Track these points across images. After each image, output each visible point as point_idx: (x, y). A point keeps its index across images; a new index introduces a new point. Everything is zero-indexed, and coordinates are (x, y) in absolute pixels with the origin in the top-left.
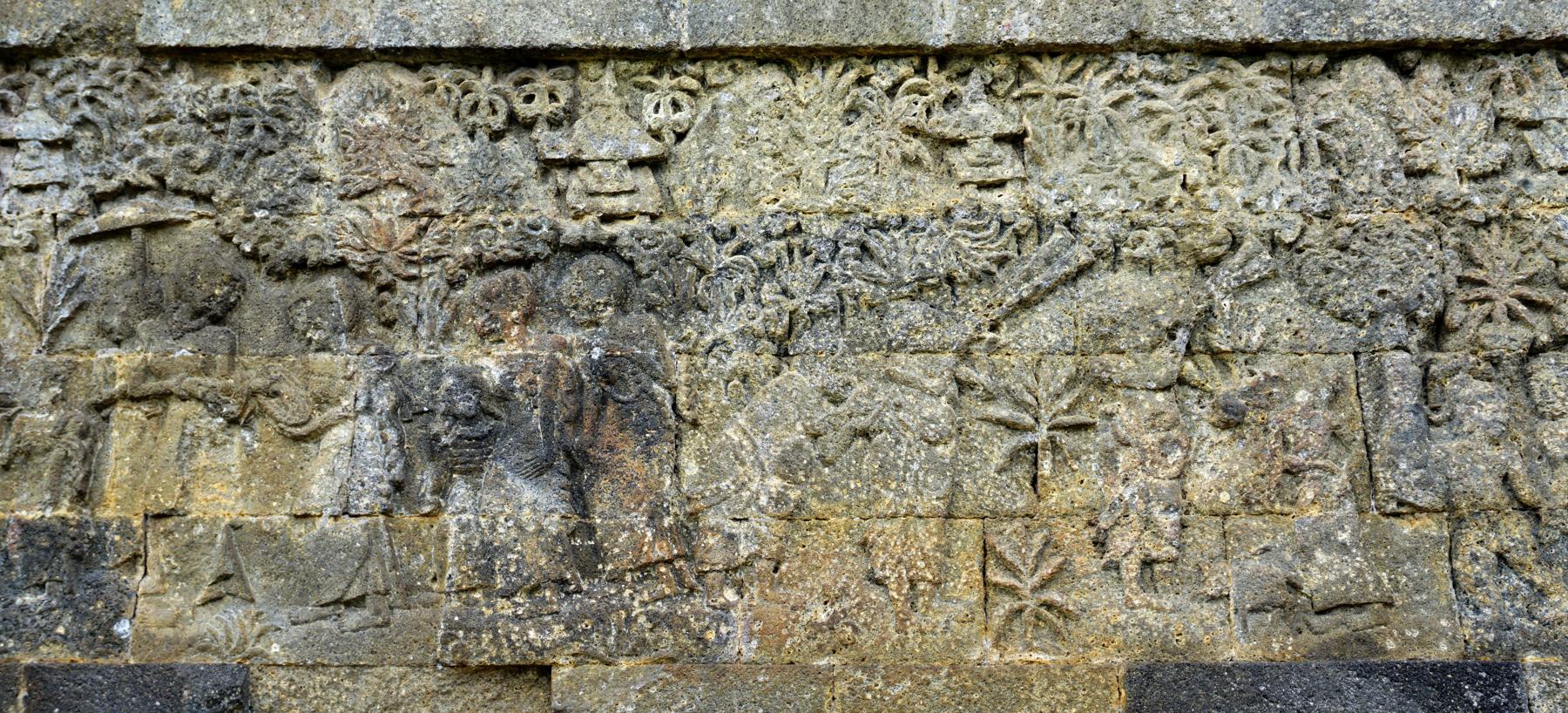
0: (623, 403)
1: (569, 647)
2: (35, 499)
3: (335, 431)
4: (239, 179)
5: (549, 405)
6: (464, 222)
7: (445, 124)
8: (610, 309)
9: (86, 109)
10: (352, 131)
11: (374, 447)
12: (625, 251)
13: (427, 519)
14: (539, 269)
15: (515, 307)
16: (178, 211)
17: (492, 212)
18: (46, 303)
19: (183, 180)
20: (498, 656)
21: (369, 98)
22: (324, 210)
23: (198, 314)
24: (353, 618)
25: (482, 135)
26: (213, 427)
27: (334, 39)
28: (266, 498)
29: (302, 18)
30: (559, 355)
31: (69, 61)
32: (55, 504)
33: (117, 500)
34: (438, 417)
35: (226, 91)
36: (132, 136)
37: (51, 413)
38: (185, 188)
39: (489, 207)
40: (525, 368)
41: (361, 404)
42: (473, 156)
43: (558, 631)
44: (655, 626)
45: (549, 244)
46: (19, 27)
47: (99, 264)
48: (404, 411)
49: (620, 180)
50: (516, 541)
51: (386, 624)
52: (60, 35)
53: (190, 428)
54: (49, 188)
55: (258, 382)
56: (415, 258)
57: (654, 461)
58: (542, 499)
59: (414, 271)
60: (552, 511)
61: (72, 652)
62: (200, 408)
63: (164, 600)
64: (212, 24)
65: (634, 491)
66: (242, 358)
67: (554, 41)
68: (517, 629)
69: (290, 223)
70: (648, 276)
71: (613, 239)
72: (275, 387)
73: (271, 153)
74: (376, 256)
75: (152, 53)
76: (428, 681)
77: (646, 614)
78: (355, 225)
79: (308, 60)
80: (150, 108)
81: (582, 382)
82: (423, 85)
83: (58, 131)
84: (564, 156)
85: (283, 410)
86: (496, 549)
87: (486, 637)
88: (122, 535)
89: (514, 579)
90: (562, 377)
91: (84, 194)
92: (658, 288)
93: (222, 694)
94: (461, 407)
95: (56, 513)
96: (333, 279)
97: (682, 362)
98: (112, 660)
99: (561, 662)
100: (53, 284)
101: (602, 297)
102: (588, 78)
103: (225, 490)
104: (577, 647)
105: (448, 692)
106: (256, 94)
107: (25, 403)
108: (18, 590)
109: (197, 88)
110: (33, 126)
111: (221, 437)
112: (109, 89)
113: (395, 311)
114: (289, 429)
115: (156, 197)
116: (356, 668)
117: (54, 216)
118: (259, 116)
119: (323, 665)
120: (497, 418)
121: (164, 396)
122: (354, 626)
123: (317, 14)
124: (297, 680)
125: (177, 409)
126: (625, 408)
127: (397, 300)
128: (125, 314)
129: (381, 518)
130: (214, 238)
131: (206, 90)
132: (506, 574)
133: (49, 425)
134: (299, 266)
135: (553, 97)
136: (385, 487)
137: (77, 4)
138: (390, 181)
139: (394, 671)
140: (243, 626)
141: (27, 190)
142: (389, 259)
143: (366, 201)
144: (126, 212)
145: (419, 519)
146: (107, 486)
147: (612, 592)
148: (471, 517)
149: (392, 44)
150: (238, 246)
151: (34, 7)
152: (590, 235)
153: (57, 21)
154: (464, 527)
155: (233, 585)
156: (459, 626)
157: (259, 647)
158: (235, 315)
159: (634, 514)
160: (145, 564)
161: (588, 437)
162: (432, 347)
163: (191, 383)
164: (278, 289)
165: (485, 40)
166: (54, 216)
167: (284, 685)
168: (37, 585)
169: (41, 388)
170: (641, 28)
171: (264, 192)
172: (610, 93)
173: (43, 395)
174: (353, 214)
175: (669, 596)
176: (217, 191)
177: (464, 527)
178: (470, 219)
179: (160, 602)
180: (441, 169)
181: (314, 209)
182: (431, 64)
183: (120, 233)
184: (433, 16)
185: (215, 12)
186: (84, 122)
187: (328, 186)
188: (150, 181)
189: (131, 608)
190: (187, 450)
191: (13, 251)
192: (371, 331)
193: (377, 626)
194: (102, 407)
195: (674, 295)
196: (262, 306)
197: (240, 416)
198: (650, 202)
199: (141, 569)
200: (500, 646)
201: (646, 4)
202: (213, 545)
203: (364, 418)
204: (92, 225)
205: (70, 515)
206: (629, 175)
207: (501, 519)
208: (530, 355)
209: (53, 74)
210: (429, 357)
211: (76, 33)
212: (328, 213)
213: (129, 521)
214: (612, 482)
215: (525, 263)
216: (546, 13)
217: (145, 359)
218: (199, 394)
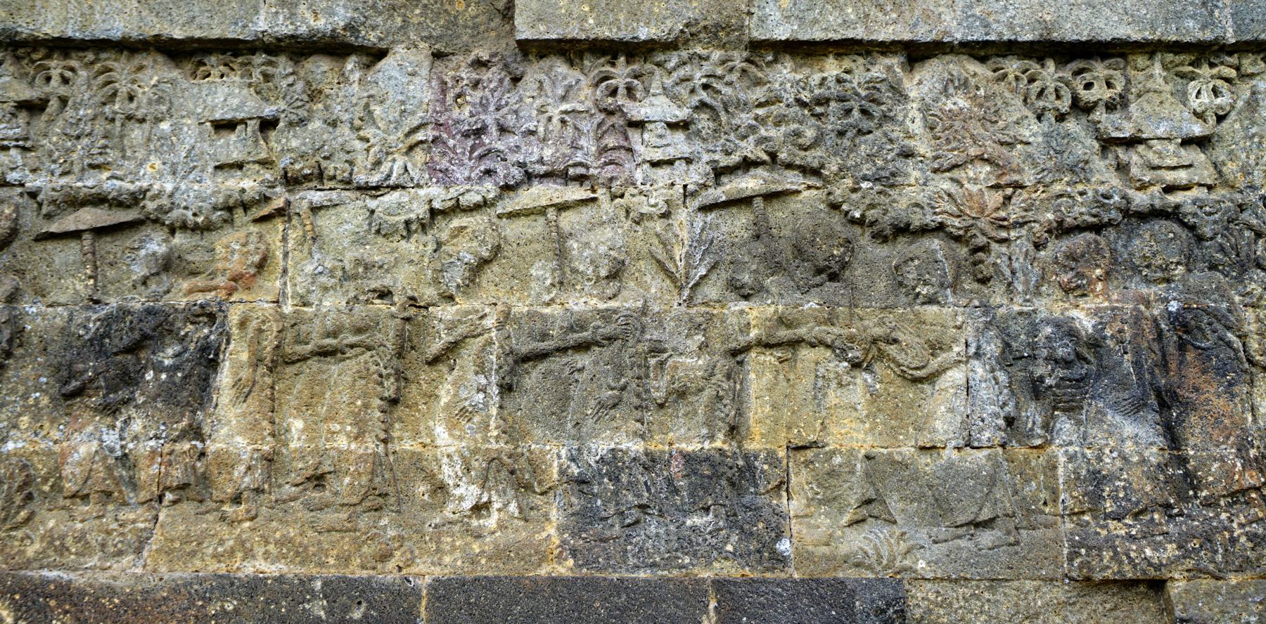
0: (1203, 349)
1: (1183, 564)
2: (691, 433)
3: (949, 373)
4: (845, 155)
5: (1137, 353)
6: (1043, 192)
7: (1017, 109)
8: (1180, 267)
9: (704, 95)
10: (939, 113)
11: (988, 387)
12: (1189, 217)
13: (1035, 451)
14: (1111, 233)
15: (1098, 266)
16: (792, 183)
17: (1068, 184)
18: (687, 262)
19: (795, 156)
20: (1119, 572)
21: (950, 85)
22: (921, 182)
23: (819, 271)
24: (986, 538)
25: (1050, 116)
26: (840, 370)
27: (924, 34)
28: (893, 432)
29: (894, 15)
30: (1142, 307)
31: (684, 54)
32: (712, 437)
33: (762, 434)
34: (1040, 361)
35: (824, 79)
36: (745, 118)
37: (699, 358)
38: (797, 163)
39: (1066, 179)
40: (1114, 318)
41: (972, 350)
42: (1045, 135)
43: (1171, 550)
44: (1255, 546)
45: (1121, 211)
46: (647, 24)
47: (724, 229)
48: (1009, 358)
49: (1176, 154)
50: (1121, 470)
51: (1017, 543)
52: (682, 31)
53: (822, 371)
54: (677, 163)
55: (878, 331)
56: (1006, 223)
57: (1237, 400)
58: (1142, 433)
59: (1004, 234)
60: (1151, 444)
61: (743, 568)
62: (828, 353)
63: (812, 522)
64: (815, 21)
65: (1221, 426)
66: (856, 310)
67: (1116, 36)
68: (1134, 547)
69: (891, 193)
70: (1212, 239)
71: (1177, 207)
72: (894, 335)
73: (870, 132)
74: (971, 222)
75: (757, 46)
76: (1059, 593)
77: (1247, 534)
78: (949, 195)
79: (895, 53)
80: (759, 94)
81: (1161, 330)
82: (990, 74)
83: (682, 114)
84: (1127, 135)
85: (903, 356)
86: (1104, 477)
87: (1107, 555)
88: (770, 464)
89: (1123, 504)
90: (1147, 326)
91: (708, 168)
92: (1222, 249)
93: (888, 605)
94: (1061, 352)
95: (713, 445)
96: (936, 241)
97: (1250, 314)
98: (779, 575)
99: (1176, 576)
100: (690, 246)
101: (1174, 257)
102: (1136, 69)
103: (853, 425)
104: (1190, 563)
105: (1074, 603)
106: (851, 82)
107: (674, 349)
108: (686, 513)
109: (798, 77)
110: (659, 109)
111: (846, 379)
112: (720, 78)
113: (991, 269)
114: (910, 372)
115: (768, 171)
116: (995, 582)
117: (685, 186)
118: (855, 100)
119: (966, 579)
120: (1088, 362)
121: (795, 344)
122: (990, 545)
123: (907, 13)
124: (942, 592)
125: (806, 353)
126: (1204, 354)
127: (991, 260)
128: (756, 272)
129: (1000, 450)
130: (822, 206)
131: (807, 78)
132: (1115, 499)
133: (699, 369)
134: (902, 230)
135: (1109, 85)
136: (1001, 422)
137: (695, 4)
138: (976, 157)
139: (1029, 585)
140: (890, 545)
141: (655, 164)
142: (983, 223)
143: (956, 174)
144: (750, 183)
145: (1028, 451)
146: (751, 422)
147: (1211, 515)
148: (1077, 449)
149: (975, 38)
150: (847, 213)
151: (659, 7)
152: (1158, 203)
153: (680, 19)
154: (1071, 458)
155: (875, 509)
156: (1081, 544)
157: (907, 563)
158: (847, 273)
159: (1224, 447)
160: (787, 490)
161: (1176, 379)
162: (1028, 301)
163: (821, 332)
164: (882, 251)
165: (1055, 35)
166: (685, 186)
167: (932, 596)
168: (703, 508)
169: (687, 337)
170: (1191, 24)
171: (868, 166)
172: (1161, 81)
173: (689, 342)
174: (947, 186)
175: (1262, 519)
176: (827, 165)
177: (1071, 458)
178: (1050, 189)
179: (810, 523)
180: (1019, 146)
181: (912, 181)
182: (998, 56)
183: (743, 202)
184: (1008, 14)
185: (817, 11)
186: (703, 106)
187: (921, 161)
188: (765, 157)
189: (788, 528)
190: (819, 393)
191: (650, 217)
192: (967, 287)
193: (1010, 545)
194: (737, 354)
195: (1238, 255)
196: (870, 264)
197: (863, 361)
198: (1208, 176)
199: (784, 494)
200: (1121, 563)
201: (1192, 4)
202: (854, 473)
203: (975, 363)
204: (719, 193)
205: (726, 447)
206: (1183, 152)
207: (1107, 451)
208: (1117, 308)
209: (671, 64)
210: (1026, 309)
211: (694, 30)
212: (925, 184)
213: (774, 452)
214: (1201, 418)
215: (1097, 228)
216: (1107, 12)
217: (776, 311)
218: (829, 341)
